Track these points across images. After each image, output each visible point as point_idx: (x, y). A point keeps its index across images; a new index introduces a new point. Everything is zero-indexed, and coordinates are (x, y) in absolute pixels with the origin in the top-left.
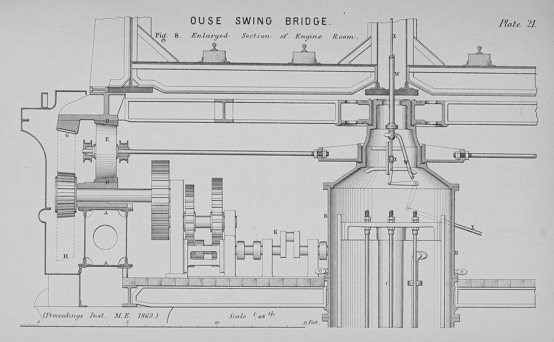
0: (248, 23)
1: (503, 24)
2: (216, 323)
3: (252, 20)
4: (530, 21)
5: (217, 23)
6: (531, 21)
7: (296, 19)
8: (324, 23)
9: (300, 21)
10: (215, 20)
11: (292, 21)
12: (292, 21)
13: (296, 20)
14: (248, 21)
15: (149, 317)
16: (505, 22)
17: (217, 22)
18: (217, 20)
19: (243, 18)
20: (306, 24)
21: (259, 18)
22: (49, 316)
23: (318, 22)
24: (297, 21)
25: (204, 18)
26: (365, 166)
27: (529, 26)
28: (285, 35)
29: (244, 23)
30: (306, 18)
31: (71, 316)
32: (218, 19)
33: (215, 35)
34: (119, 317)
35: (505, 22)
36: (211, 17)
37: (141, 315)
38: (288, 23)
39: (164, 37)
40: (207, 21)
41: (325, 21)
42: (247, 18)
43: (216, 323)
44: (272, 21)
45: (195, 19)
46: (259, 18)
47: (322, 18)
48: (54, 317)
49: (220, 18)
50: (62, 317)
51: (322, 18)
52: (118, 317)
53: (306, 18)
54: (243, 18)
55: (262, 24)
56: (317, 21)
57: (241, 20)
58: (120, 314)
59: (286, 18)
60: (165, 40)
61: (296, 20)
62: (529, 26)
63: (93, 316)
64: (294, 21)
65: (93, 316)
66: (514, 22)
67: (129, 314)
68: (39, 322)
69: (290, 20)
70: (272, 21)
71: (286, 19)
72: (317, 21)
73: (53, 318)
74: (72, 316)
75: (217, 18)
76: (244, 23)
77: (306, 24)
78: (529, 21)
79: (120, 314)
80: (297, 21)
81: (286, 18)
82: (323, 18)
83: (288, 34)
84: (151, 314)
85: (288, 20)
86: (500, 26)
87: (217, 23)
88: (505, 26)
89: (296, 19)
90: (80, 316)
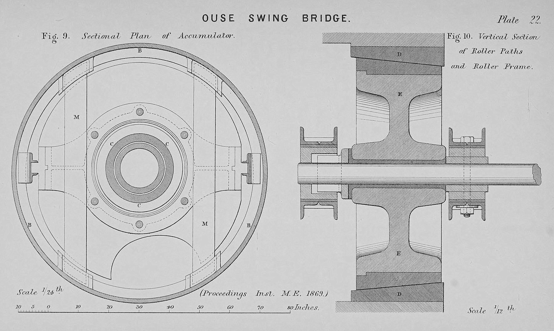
0: (263, 20)
1: (502, 21)
2: (77, 307)
3: (266, 17)
4: (533, 17)
5: (230, 21)
6: (540, 17)
7: (313, 17)
8: (231, 19)
9: (318, 18)
10: (227, 18)
11: (309, 17)
12: (309, 17)
13: (314, 17)
14: (276, 18)
15: (319, 292)
16: (504, 18)
17: (230, 19)
18: (230, 18)
19: (258, 15)
20: (326, 21)
21: (274, 16)
22: (207, 294)
23: (338, 19)
24: (315, 18)
25: (321, 15)
26: (46, 170)
27: (532, 23)
28: (168, 35)
29: (259, 20)
30: (326, 16)
31: (233, 294)
32: (344, 17)
33: (489, 36)
34: (287, 295)
35: (504, 18)
36: (223, 14)
37: (310, 293)
38: (305, 19)
39: (54, 38)
40: (219, 18)
41: (232, 18)
42: (261, 15)
43: (77, 307)
44: (339, 18)
45: (208, 17)
46: (274, 16)
47: (326, 21)
48: (214, 295)
49: (233, 15)
50: (220, 294)
51: (326, 21)
52: (287, 295)
53: (326, 16)
54: (258, 15)
55: (278, 21)
56: (285, 19)
57: (255, 18)
58: (288, 292)
59: (303, 15)
60: (56, 42)
61: (314, 17)
62: (532, 23)
63: (259, 294)
64: (312, 18)
65: (259, 294)
66: (513, 18)
67: (299, 291)
68: (49, 307)
69: (316, 17)
70: (339, 18)
71: (312, 16)
72: (285, 19)
73: (21, 305)
74: (235, 294)
75: (230, 15)
76: (259, 20)
77: (326, 21)
78: (532, 17)
79: (288, 292)
80: (315, 18)
81: (303, 15)
82: (343, 15)
83: (170, 33)
84: (321, 292)
85: (305, 18)
86: (499, 22)
87: (230, 21)
88: (504, 22)
89: (315, 16)
90: (243, 294)
